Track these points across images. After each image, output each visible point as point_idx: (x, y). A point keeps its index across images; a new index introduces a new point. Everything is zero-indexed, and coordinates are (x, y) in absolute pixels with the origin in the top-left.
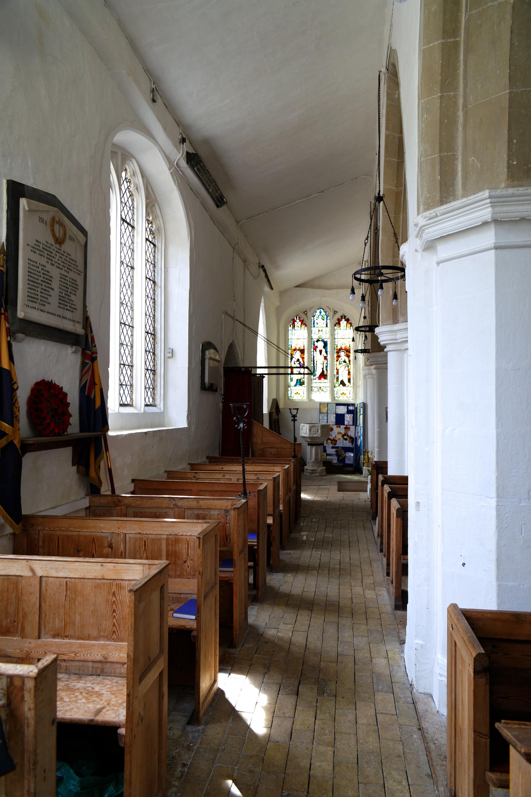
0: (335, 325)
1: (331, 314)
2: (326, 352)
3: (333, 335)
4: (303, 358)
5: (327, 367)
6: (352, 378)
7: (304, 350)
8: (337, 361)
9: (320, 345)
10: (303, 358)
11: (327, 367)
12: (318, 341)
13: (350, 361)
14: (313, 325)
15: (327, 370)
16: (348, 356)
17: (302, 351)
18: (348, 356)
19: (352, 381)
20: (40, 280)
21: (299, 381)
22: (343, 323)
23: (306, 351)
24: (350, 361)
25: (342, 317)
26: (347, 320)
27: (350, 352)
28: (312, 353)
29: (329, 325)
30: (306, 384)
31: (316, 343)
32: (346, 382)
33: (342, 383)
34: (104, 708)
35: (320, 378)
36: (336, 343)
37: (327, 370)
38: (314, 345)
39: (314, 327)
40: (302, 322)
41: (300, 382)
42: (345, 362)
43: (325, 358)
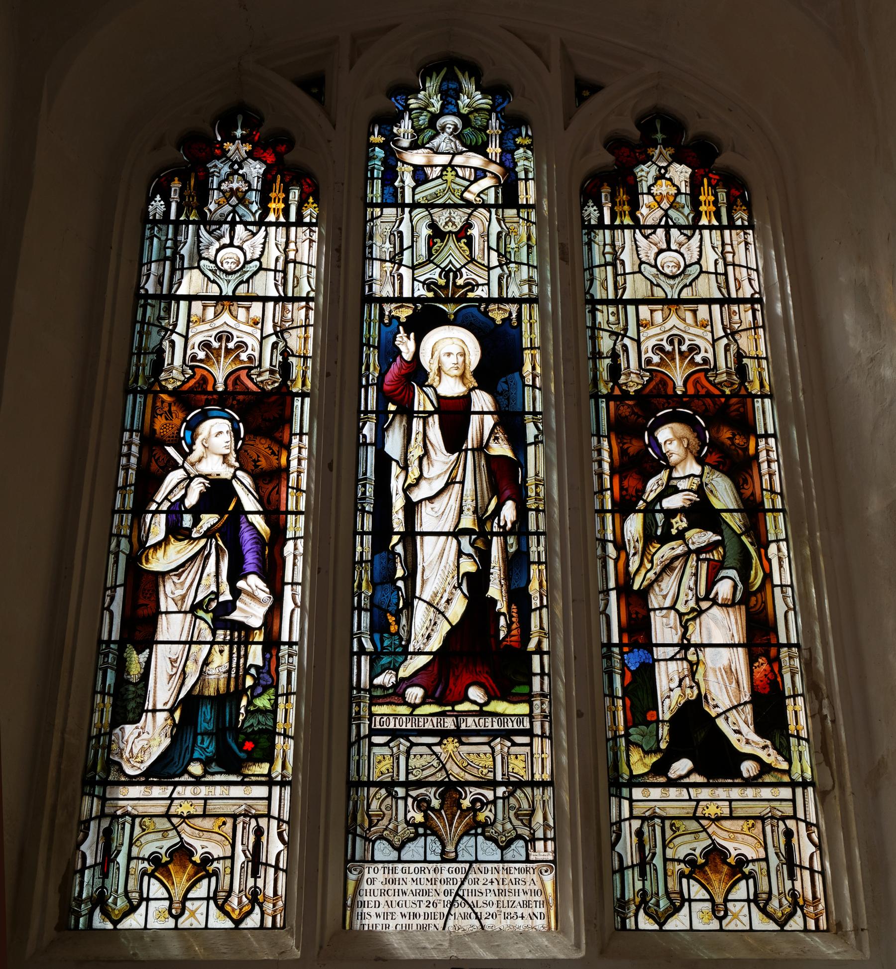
0: (590, 194)
1: (546, 90)
2: (510, 422)
3: (568, 253)
4: (270, 480)
5: (516, 564)
6: (792, 681)
7: (282, 398)
8: (623, 508)
9: (449, 353)
10: (270, 480)
11: (516, 564)
12: (425, 319)
13: (752, 510)
14: (376, 191)
15: (518, 596)
16: (739, 467)
17: (261, 414)
18: (739, 467)
19: (798, 715)
20: (409, 880)
21: (206, 718)
22: (665, 180)
23: (302, 412)
24: (752, 510)
25: (646, 124)
26: (701, 155)
27: (746, 426)
28: (369, 431)
29: (527, 192)
30: (284, 747)
31: (406, 346)
32: (741, 732)
33: (695, 732)
34: (795, 704)
35: (444, 677)
36: (606, 343)
37: (518, 596)
38: (390, 352)
39: (394, 200)
40: (272, 145)
41: (225, 729)
42: (702, 513)
43: (504, 478)
